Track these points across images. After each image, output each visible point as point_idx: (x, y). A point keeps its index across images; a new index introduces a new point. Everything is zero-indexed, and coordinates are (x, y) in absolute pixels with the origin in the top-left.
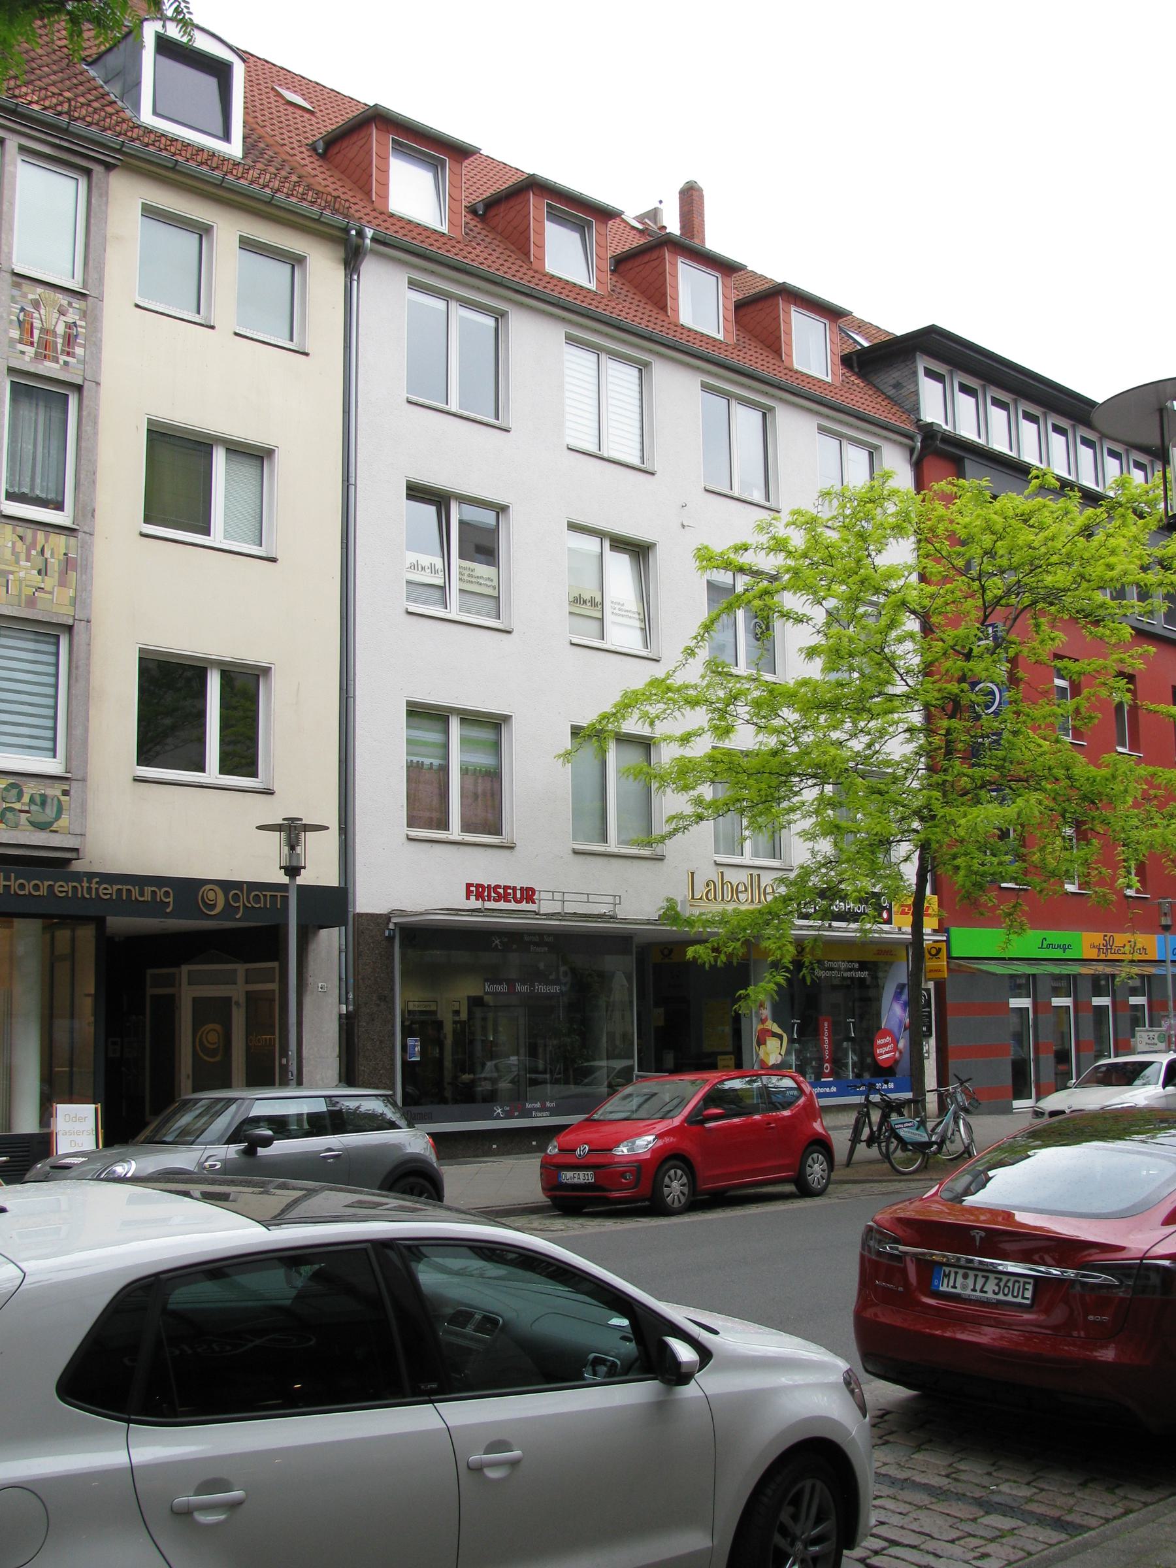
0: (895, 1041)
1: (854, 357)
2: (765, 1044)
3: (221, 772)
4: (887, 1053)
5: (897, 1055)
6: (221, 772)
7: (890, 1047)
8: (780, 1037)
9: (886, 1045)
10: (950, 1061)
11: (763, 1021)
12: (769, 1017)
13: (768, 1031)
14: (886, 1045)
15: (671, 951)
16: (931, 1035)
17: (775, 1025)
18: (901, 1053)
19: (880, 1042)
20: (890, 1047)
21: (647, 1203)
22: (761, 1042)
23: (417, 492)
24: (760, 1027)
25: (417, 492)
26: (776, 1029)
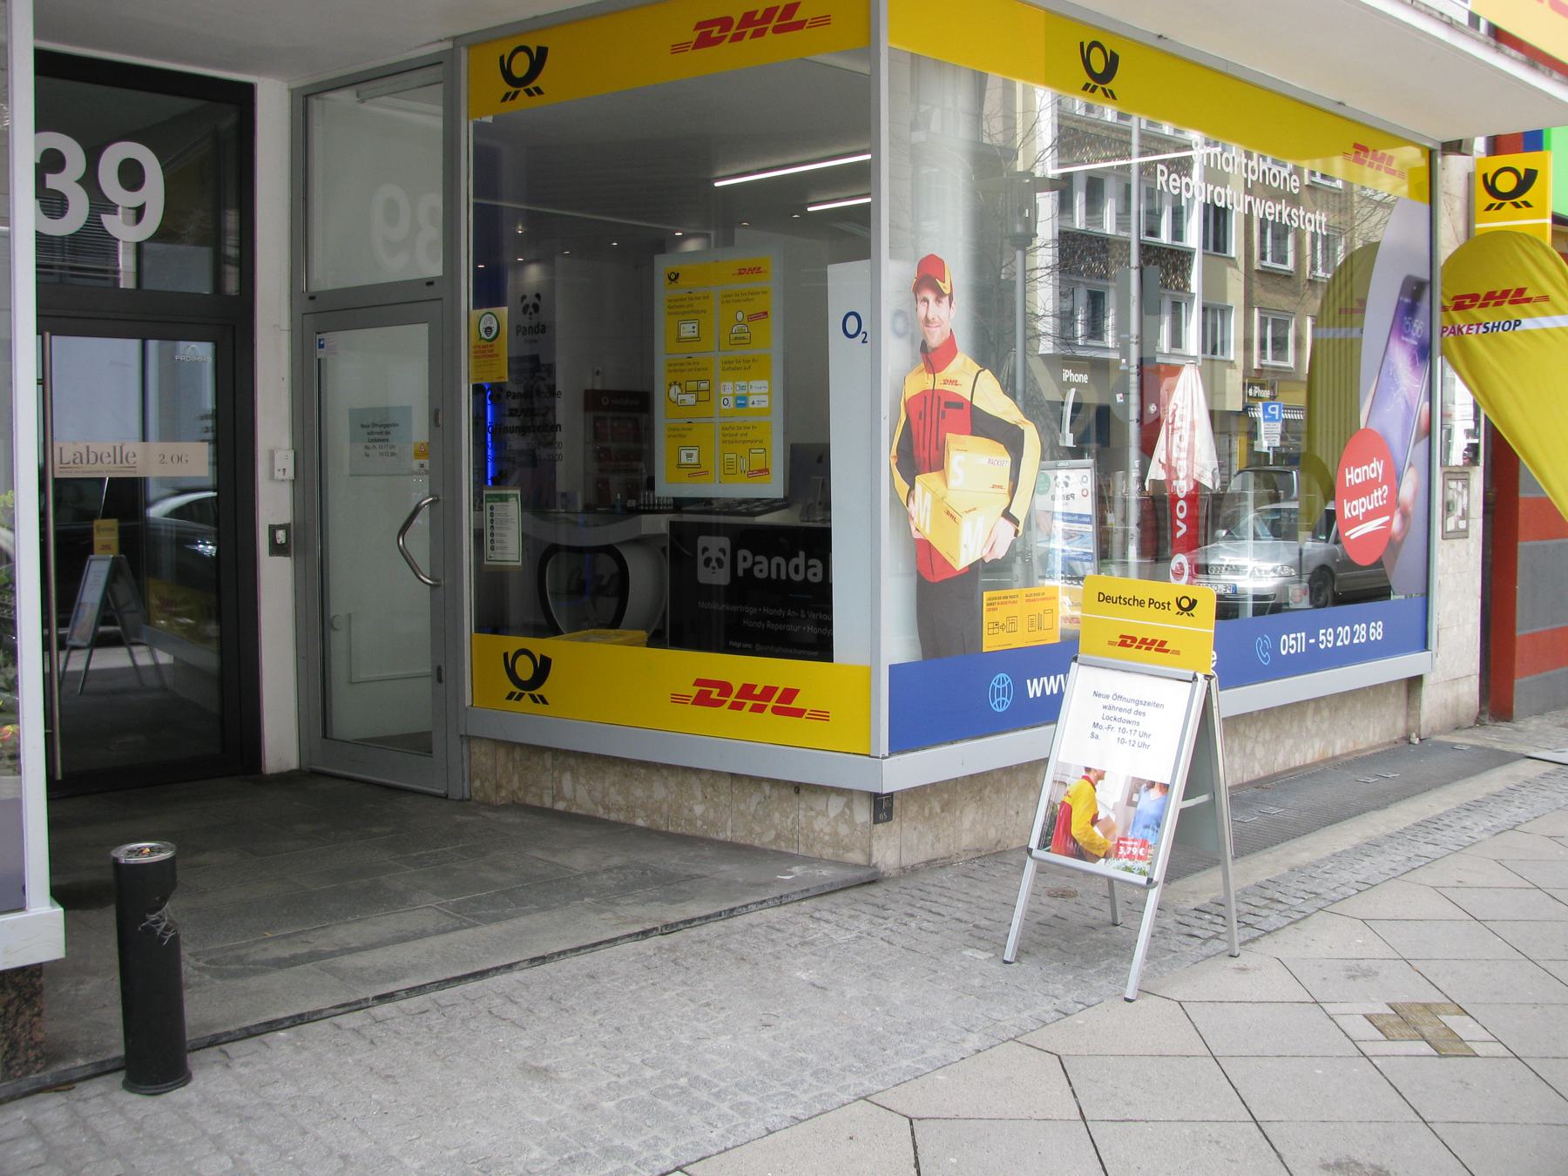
0: (1393, 478)
1: (864, 69)
2: (937, 463)
3: (891, 667)
4: (1369, 516)
5: (1396, 525)
6: (891, 667)
7: (1378, 496)
8: (1011, 439)
9: (1366, 488)
10: (1524, 546)
11: (933, 358)
12: (963, 341)
13: (957, 403)
14: (1366, 488)
15: (539, 60)
16: (1477, 464)
17: (988, 382)
18: (1405, 516)
19: (1354, 476)
20: (1378, 496)
21: (468, 703)
22: (919, 455)
23: (504, 100)
24: (920, 382)
25: (504, 100)
26: (992, 399)
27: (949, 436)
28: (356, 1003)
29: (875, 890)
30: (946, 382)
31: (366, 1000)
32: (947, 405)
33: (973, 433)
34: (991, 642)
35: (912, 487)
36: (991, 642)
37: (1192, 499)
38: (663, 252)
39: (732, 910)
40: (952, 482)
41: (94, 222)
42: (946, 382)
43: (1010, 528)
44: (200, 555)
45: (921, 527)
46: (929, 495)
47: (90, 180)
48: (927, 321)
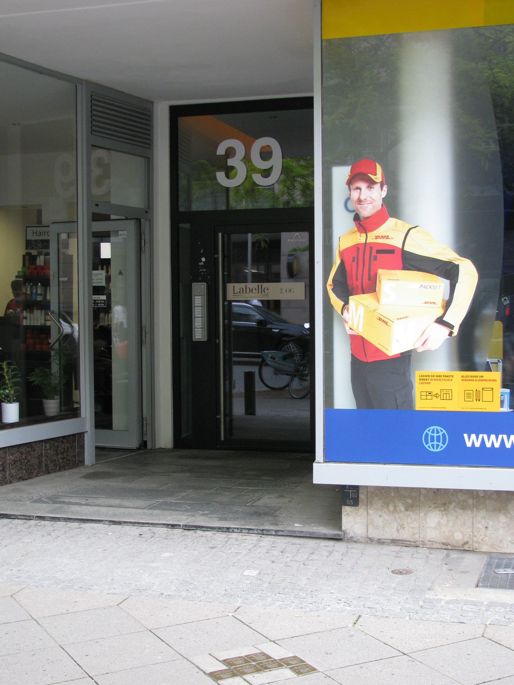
2: (370, 287)
27: (380, 271)
28: (29, 516)
29: (338, 545)
30: (377, 237)
31: (33, 516)
32: (379, 252)
33: (405, 268)
34: (421, 404)
35: (346, 303)
36: (421, 404)
37: (117, 324)
38: (110, 202)
39: (228, 528)
40: (383, 299)
41: (248, 177)
42: (377, 237)
43: (446, 331)
44: (275, 332)
45: (355, 327)
46: (361, 309)
47: (247, 159)
48: (359, 201)
